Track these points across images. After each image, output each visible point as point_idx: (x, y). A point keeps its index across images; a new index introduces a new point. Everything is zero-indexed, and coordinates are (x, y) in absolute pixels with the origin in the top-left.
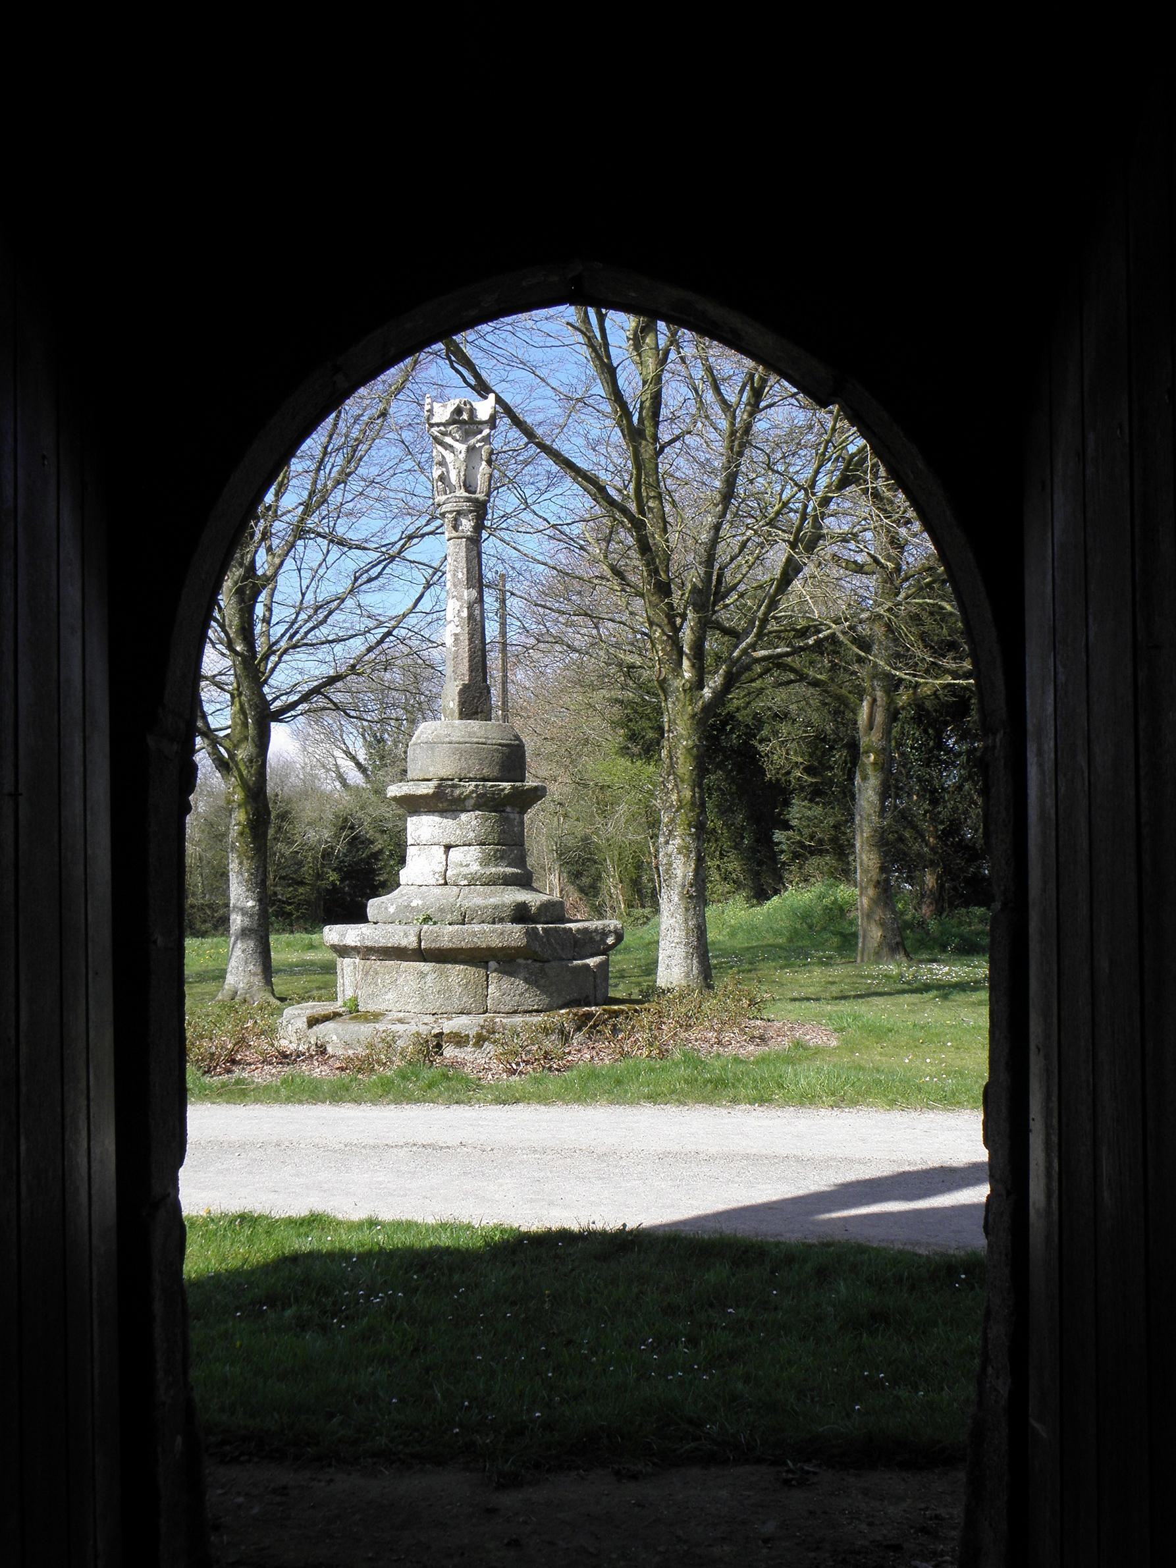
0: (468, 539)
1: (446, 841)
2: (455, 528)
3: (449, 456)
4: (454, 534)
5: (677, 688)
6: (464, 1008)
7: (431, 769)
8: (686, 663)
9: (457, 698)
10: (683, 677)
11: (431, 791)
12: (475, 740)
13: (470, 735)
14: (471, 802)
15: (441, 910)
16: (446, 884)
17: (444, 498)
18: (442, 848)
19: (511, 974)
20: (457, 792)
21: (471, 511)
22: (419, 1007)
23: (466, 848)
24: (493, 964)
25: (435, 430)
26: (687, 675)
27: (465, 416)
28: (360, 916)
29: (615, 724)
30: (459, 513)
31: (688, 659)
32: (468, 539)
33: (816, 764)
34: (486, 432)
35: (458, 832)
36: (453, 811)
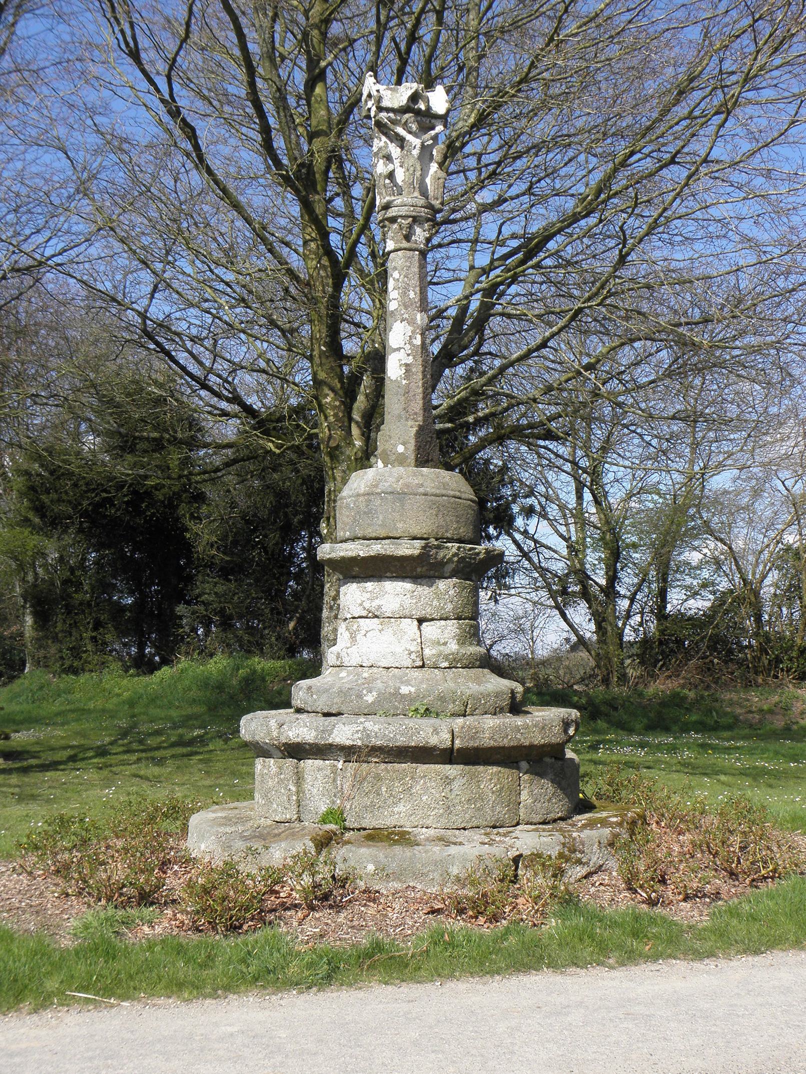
1: (418, 614)
2: (407, 238)
3: (394, 150)
5: (349, 457)
6: (497, 820)
7: (400, 525)
8: (355, 431)
9: (413, 442)
10: (354, 445)
11: (416, 552)
12: (452, 493)
13: (445, 486)
14: (451, 567)
15: (442, 699)
16: (423, 666)
18: (416, 623)
19: (541, 775)
20: (441, 554)
22: (444, 821)
23: (443, 622)
24: (524, 765)
25: (383, 115)
26: (358, 443)
28: (280, 701)
30: (416, 220)
31: (359, 426)
35: (435, 603)
36: (429, 577)
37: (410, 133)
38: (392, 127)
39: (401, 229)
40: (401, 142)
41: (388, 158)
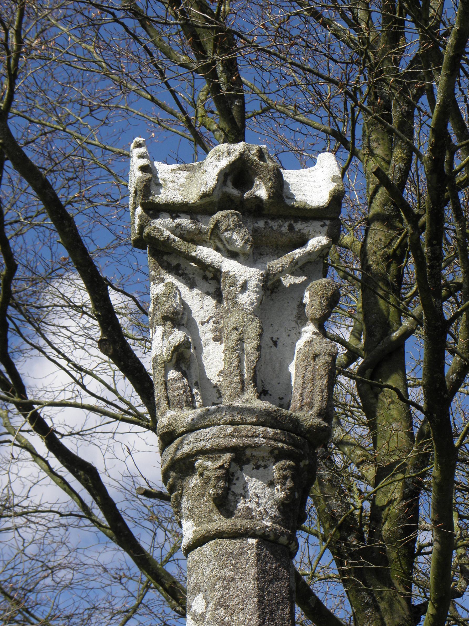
0: (264, 539)
3: (201, 306)
4: (220, 523)
17: (188, 415)
21: (278, 455)
25: (163, 225)
27: (262, 191)
29: (229, 272)
32: (264, 539)
33: (346, 370)
34: (317, 241)
37: (233, 255)
38: (184, 246)
39: (206, 483)
40: (210, 280)
41: (178, 318)
